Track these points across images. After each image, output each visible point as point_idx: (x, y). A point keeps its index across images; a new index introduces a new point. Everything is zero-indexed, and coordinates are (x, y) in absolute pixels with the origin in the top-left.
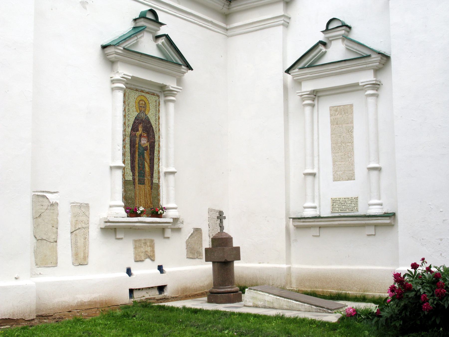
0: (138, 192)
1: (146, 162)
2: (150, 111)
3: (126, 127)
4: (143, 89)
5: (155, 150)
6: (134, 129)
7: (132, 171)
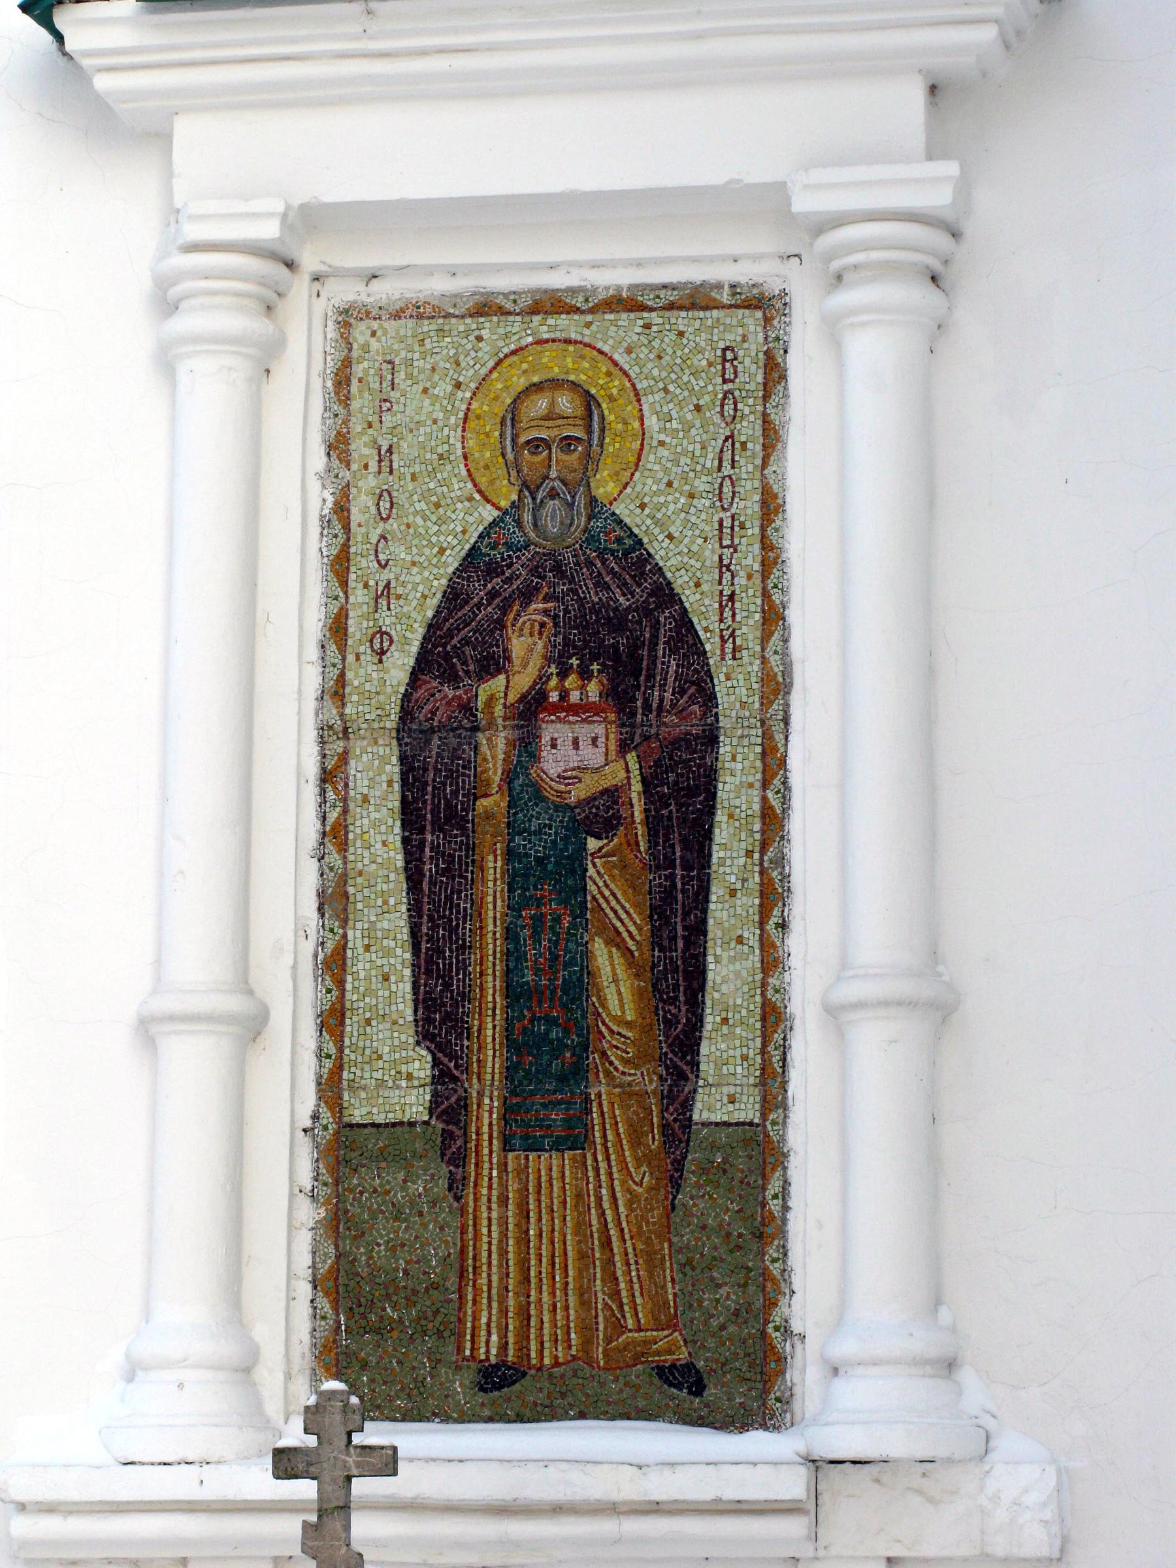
0: (504, 1222)
1: (599, 947)
2: (649, 460)
3: (351, 658)
5: (720, 816)
7: (426, 1034)
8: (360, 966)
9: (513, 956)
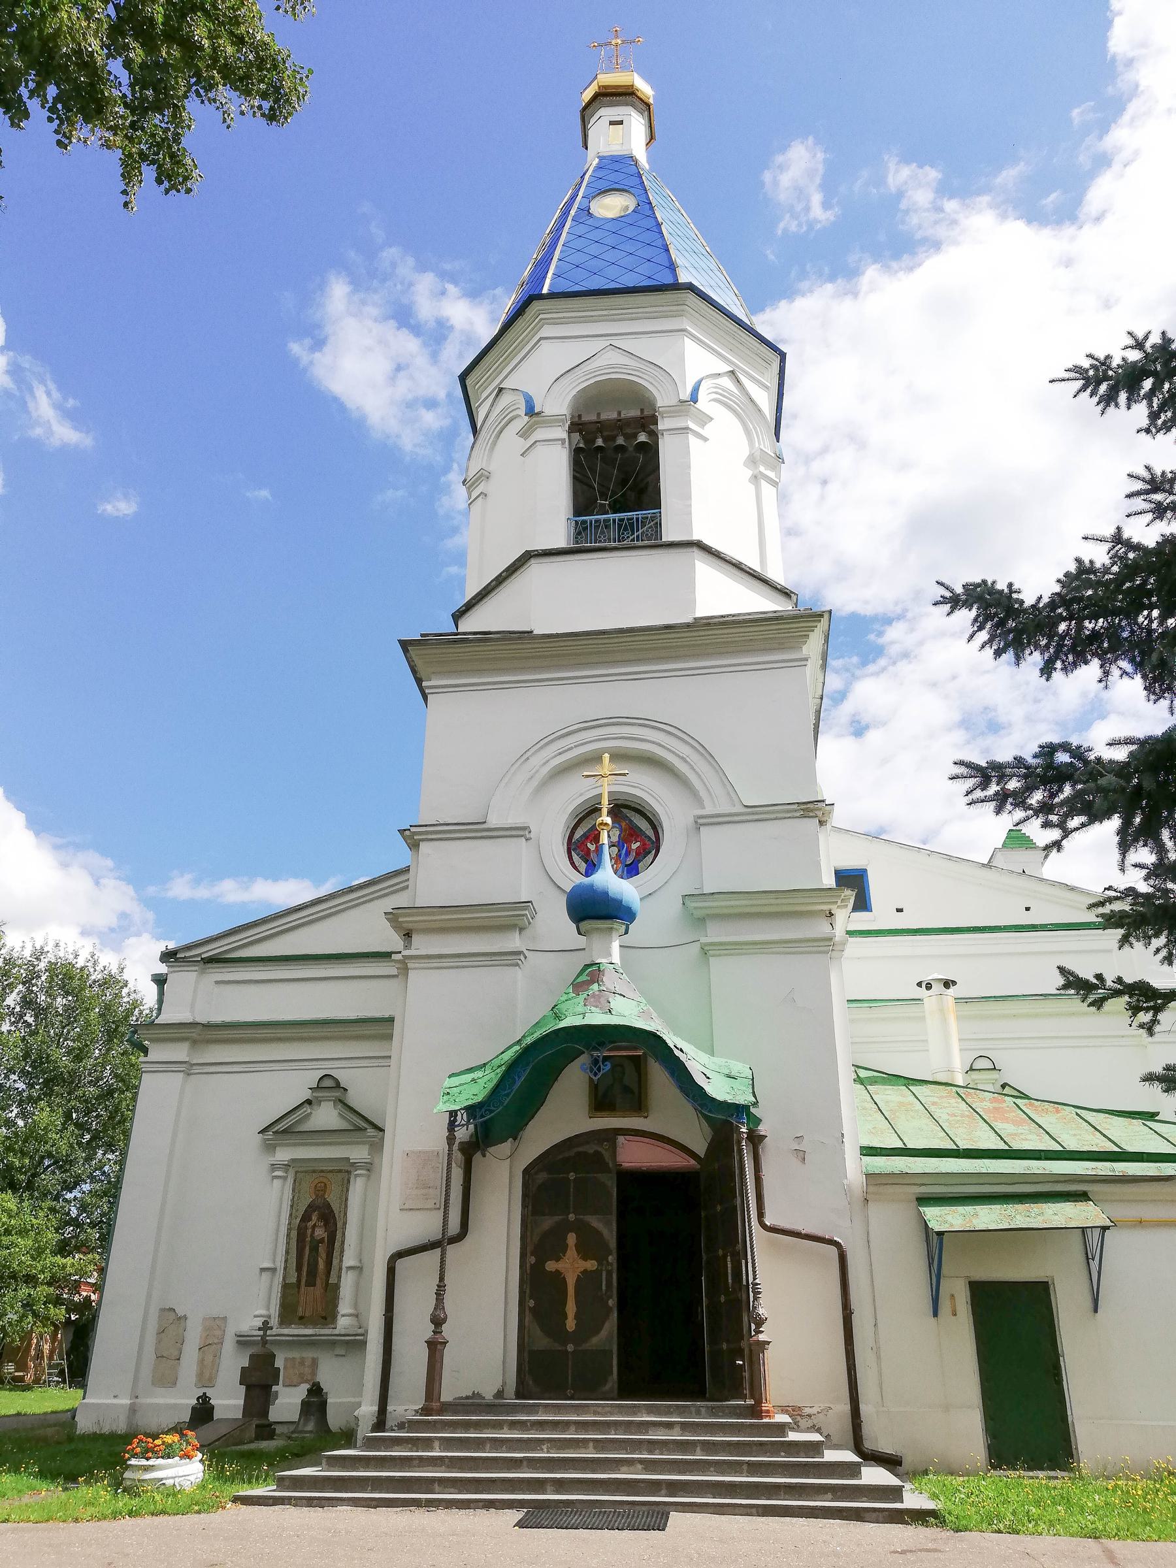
4: (321, 1168)
6: (306, 1218)
7: (297, 1270)
8: (289, 1261)
9: (309, 1260)
